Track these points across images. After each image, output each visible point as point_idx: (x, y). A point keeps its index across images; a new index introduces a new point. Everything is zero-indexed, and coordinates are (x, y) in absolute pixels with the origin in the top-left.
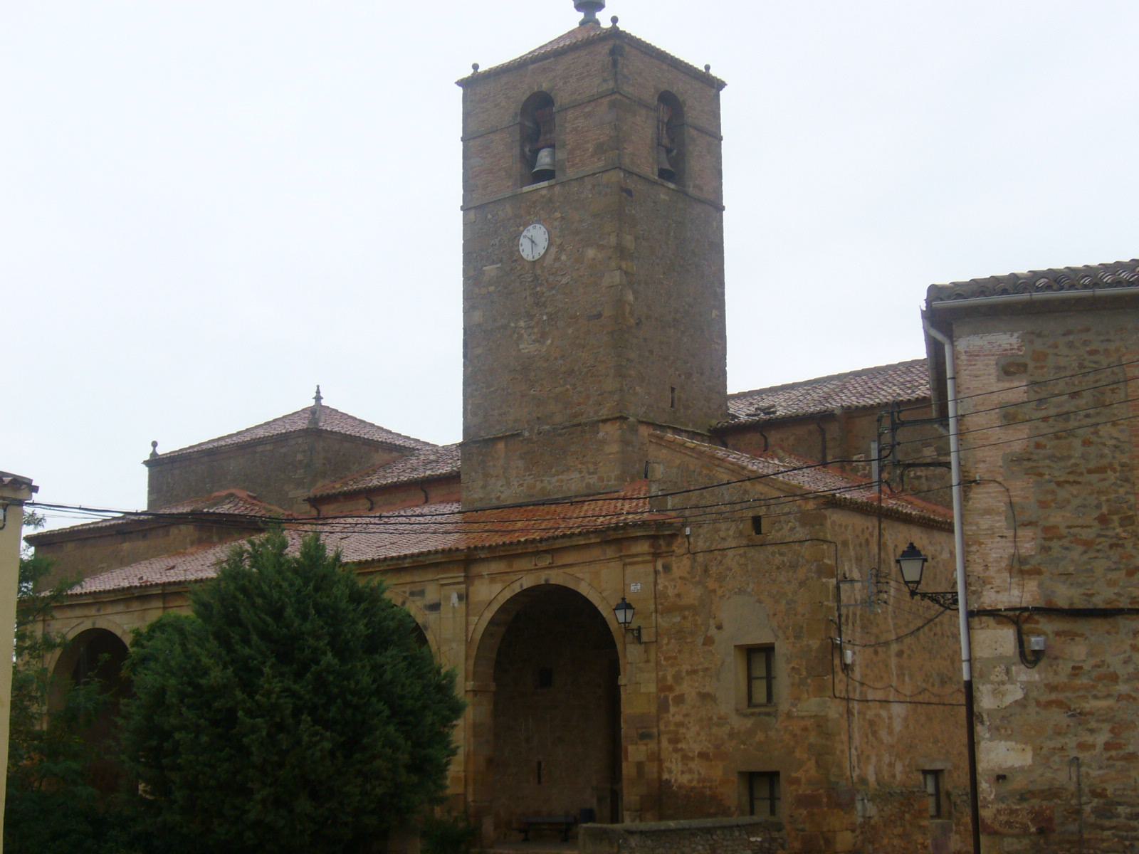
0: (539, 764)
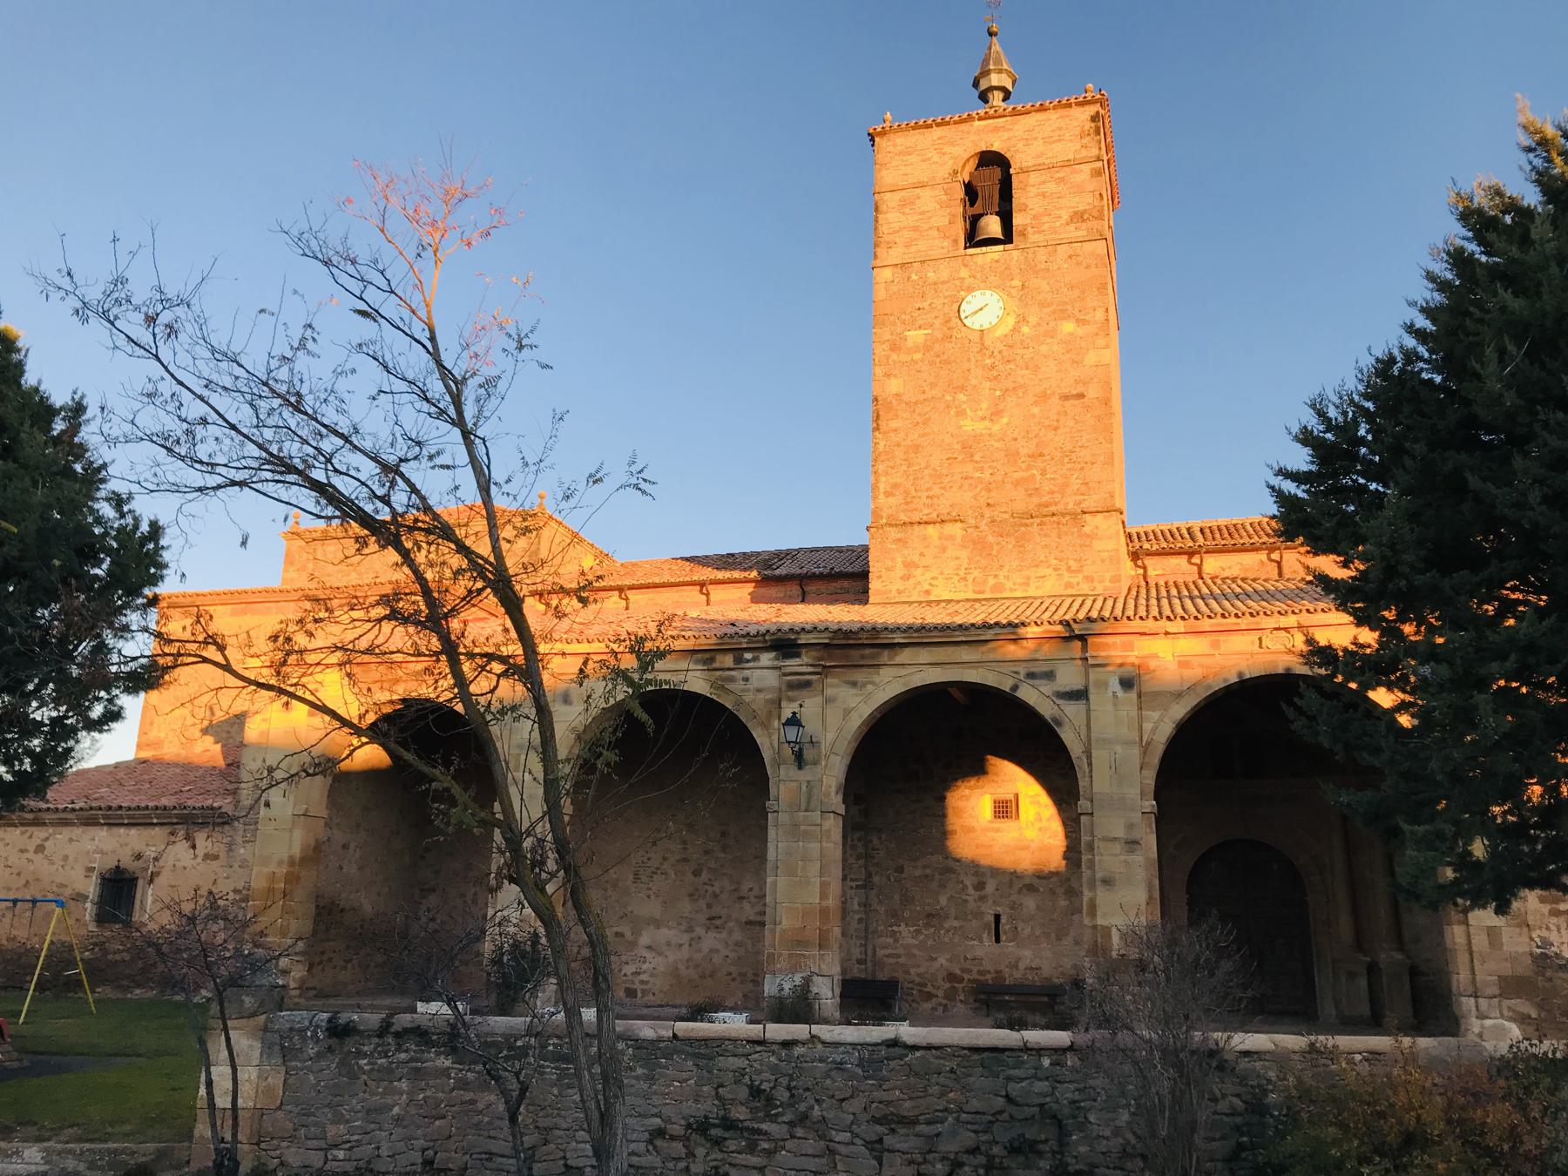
0: (997, 917)
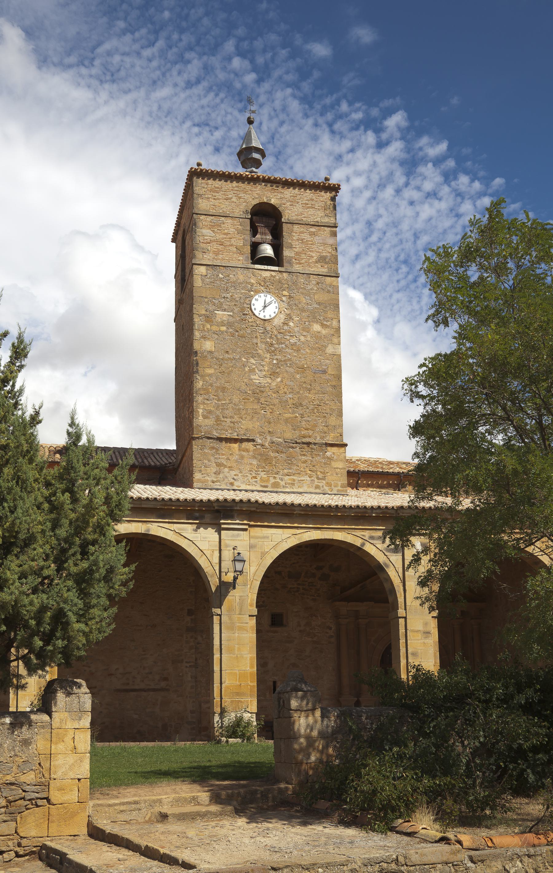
0: (275, 683)
